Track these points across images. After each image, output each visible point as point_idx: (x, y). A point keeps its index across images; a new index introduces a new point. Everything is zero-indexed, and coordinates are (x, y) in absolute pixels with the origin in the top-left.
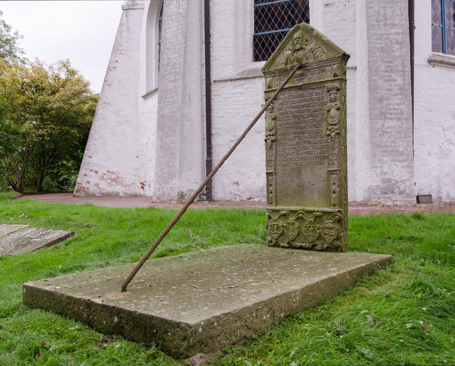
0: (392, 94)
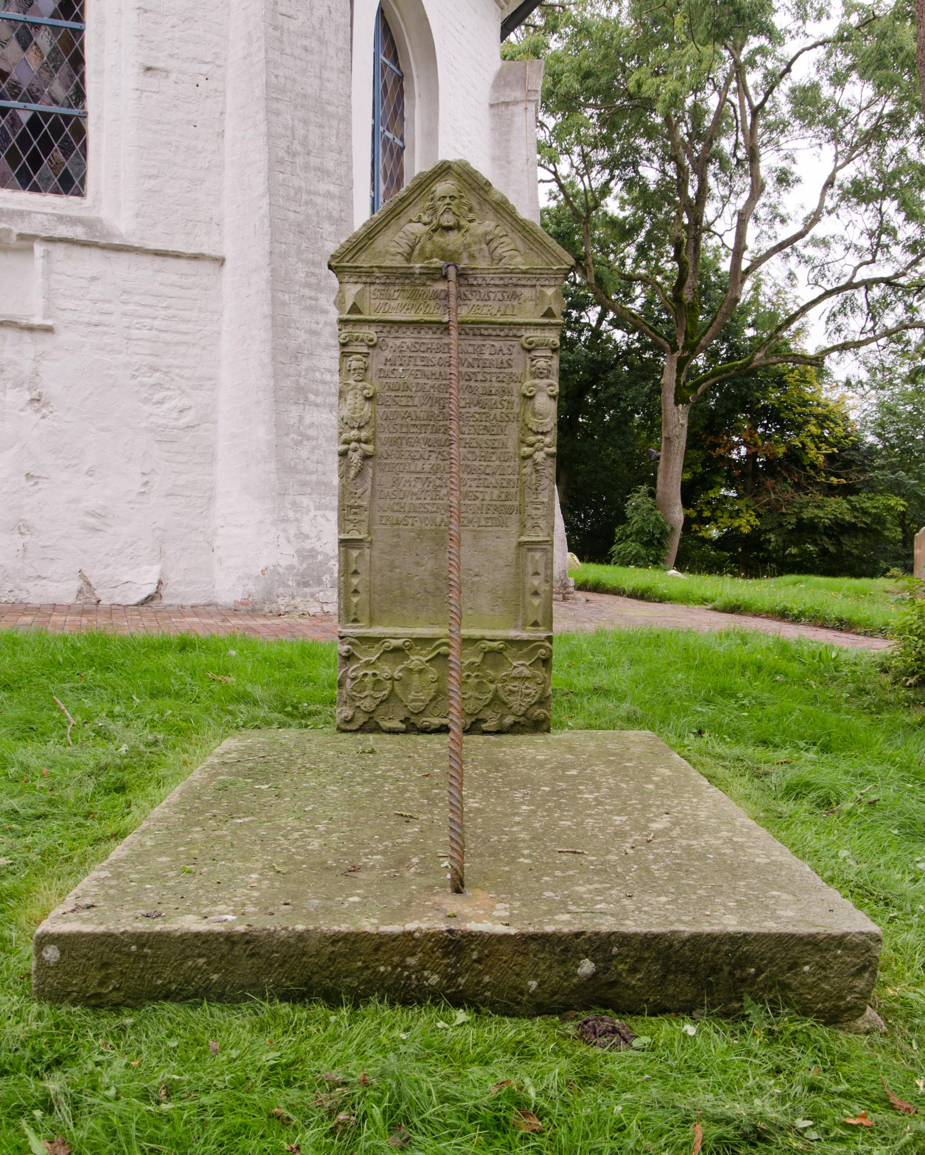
0: (318, 344)
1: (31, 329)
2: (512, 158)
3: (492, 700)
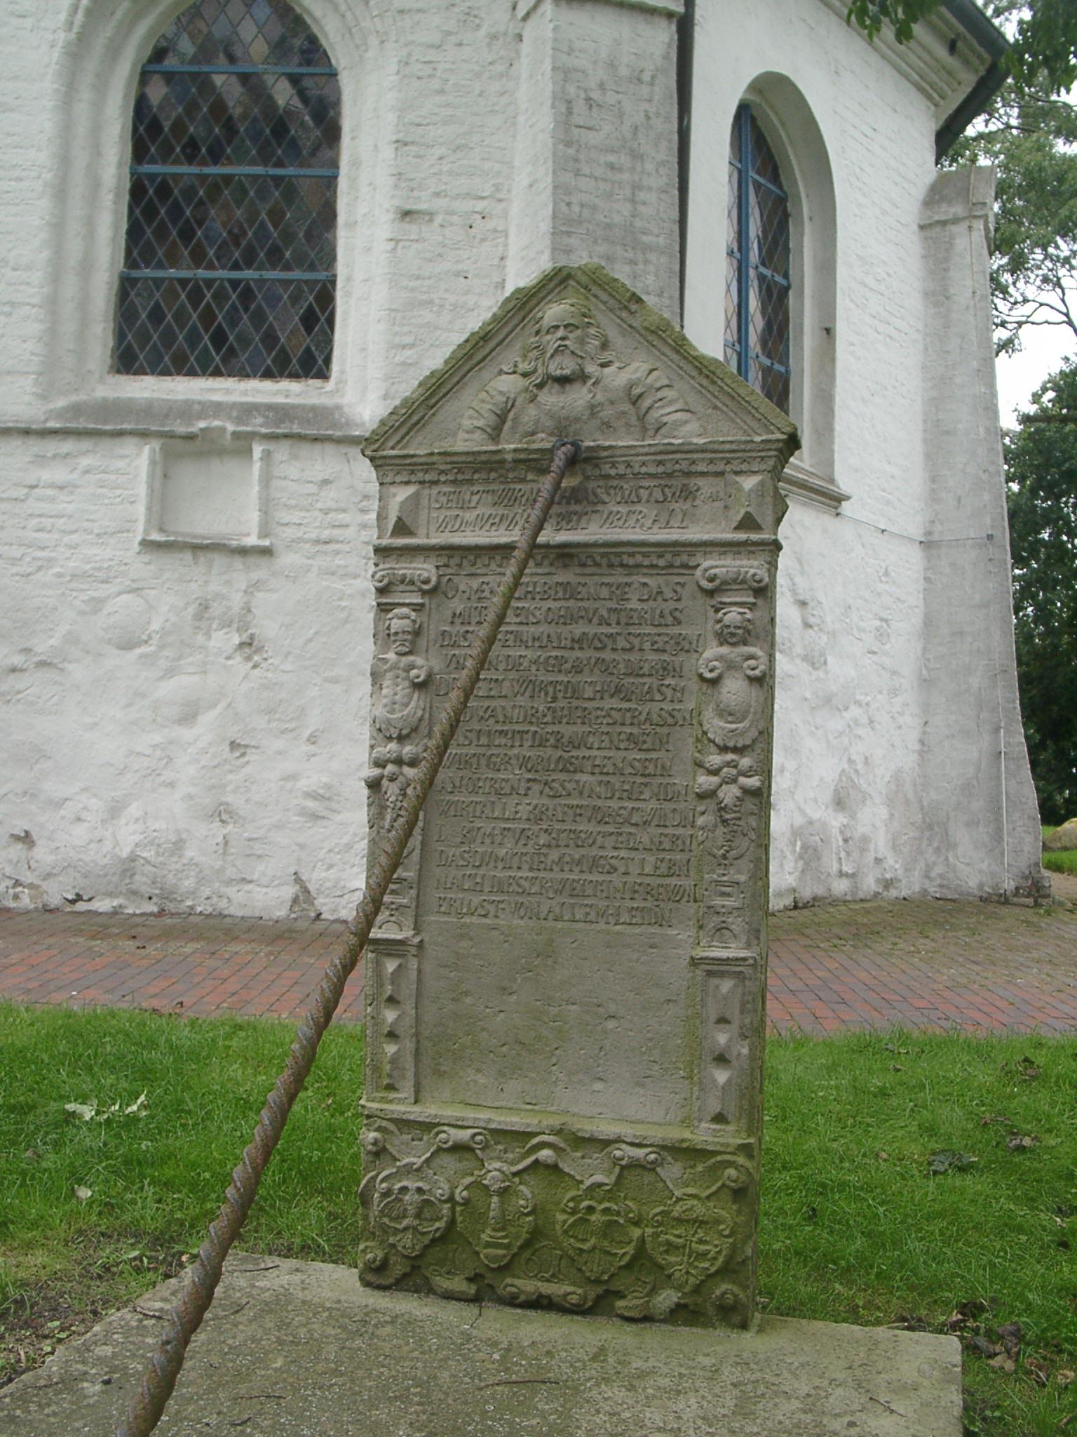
1: (243, 551)
2: (952, 291)
3: (635, 1258)
